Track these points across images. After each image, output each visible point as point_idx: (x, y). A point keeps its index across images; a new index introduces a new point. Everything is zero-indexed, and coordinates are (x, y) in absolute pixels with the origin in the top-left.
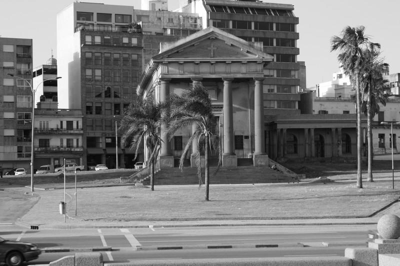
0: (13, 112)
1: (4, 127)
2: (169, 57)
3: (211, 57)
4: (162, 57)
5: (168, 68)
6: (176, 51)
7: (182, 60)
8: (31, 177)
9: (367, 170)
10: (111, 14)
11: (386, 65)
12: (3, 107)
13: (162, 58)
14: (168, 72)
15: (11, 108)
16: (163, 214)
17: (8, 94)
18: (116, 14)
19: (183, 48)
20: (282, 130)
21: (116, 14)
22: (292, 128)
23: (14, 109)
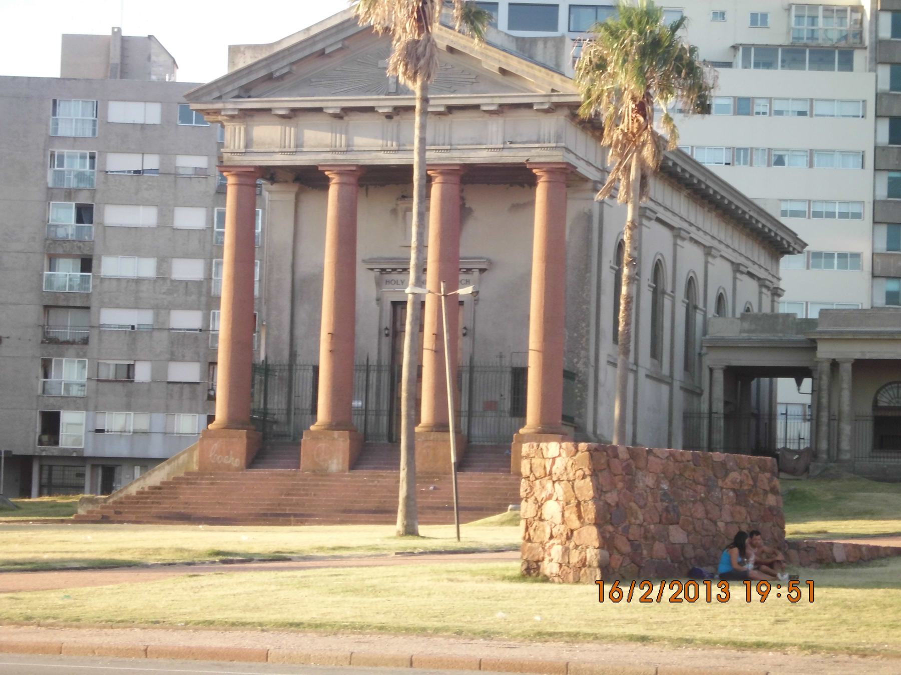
0: (198, 309)
1: (168, 356)
2: (246, 91)
3: (389, 94)
4: (216, 94)
5: (247, 133)
6: (263, 73)
7: (283, 102)
8: (30, 497)
9: (398, 468)
10: (557, 6)
11: (113, 28)
12: (169, 292)
13: (220, 97)
14: (247, 146)
15: (194, 297)
16: (573, 653)
17: (187, 255)
18: (571, 6)
19: (285, 63)
20: (835, 365)
21: (571, 6)
22: (868, 356)
23: (203, 299)
